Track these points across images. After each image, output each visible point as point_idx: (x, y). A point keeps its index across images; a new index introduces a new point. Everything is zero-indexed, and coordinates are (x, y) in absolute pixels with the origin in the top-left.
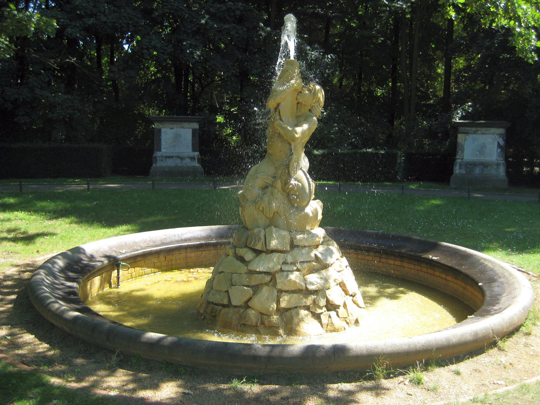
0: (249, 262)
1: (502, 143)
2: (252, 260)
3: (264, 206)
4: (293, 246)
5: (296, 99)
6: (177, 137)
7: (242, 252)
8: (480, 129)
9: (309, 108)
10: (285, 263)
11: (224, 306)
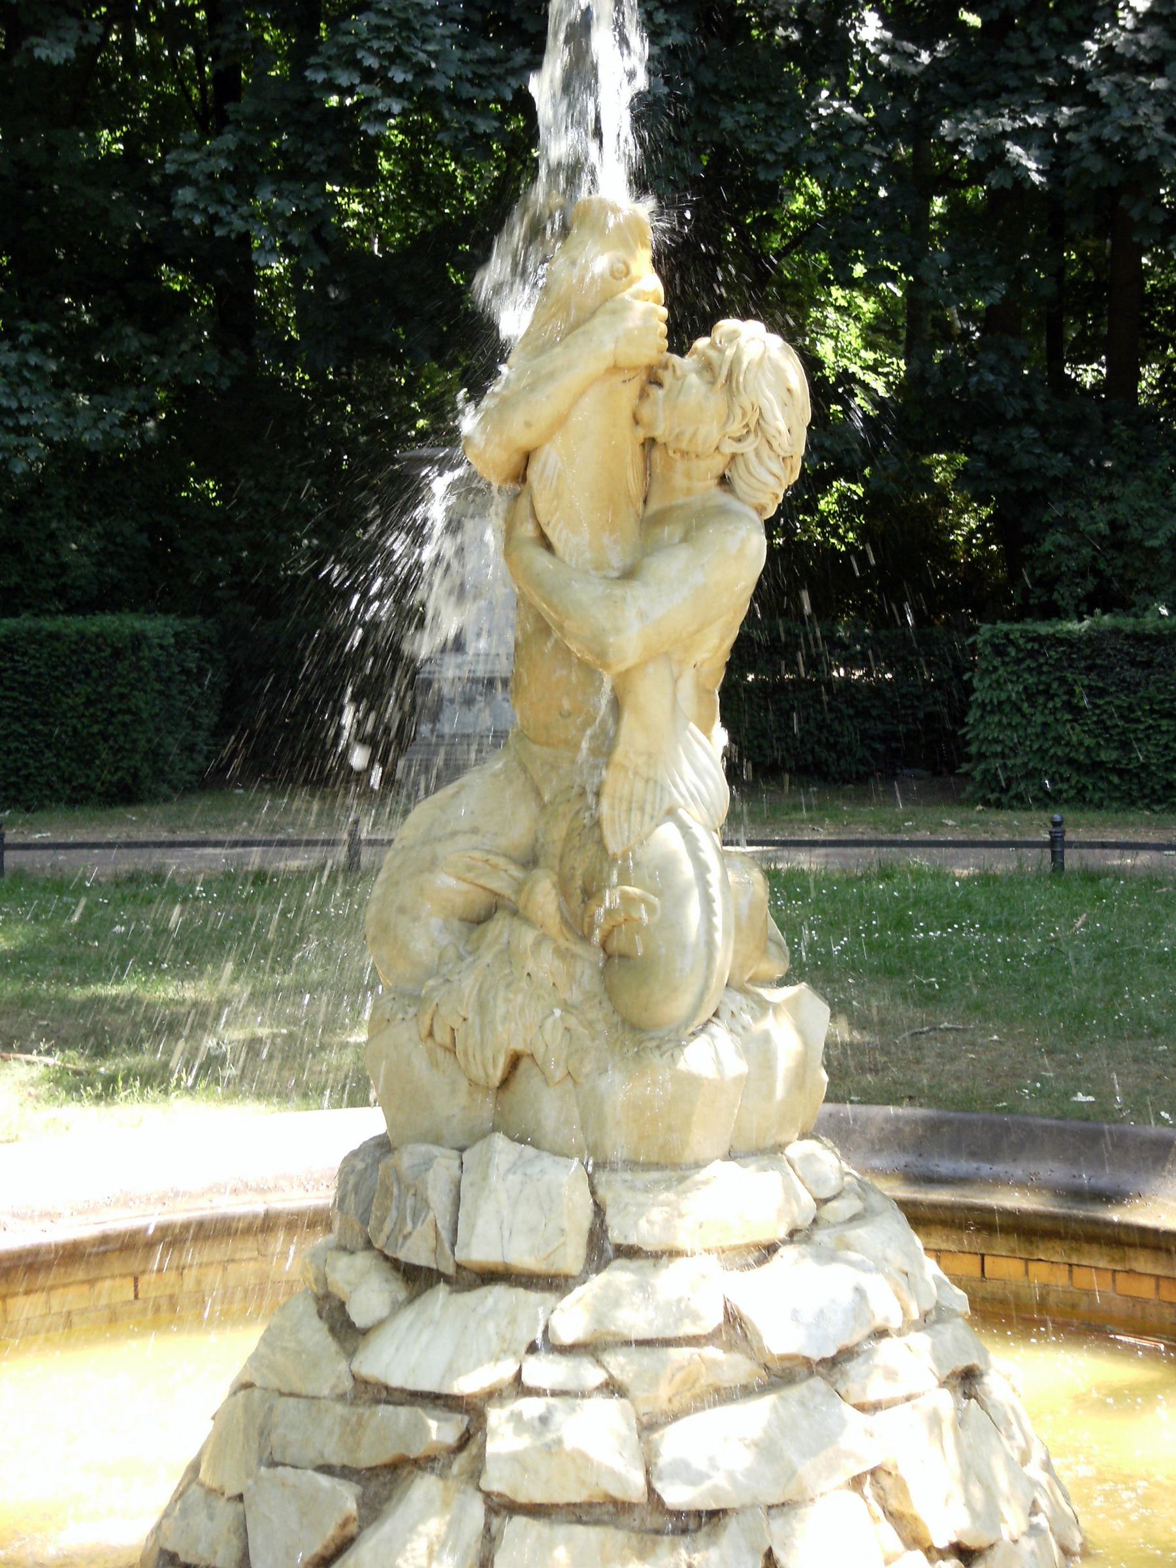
0: (365, 1332)
3: (457, 1023)
4: (602, 1249)
5: (636, 421)
9: (717, 464)
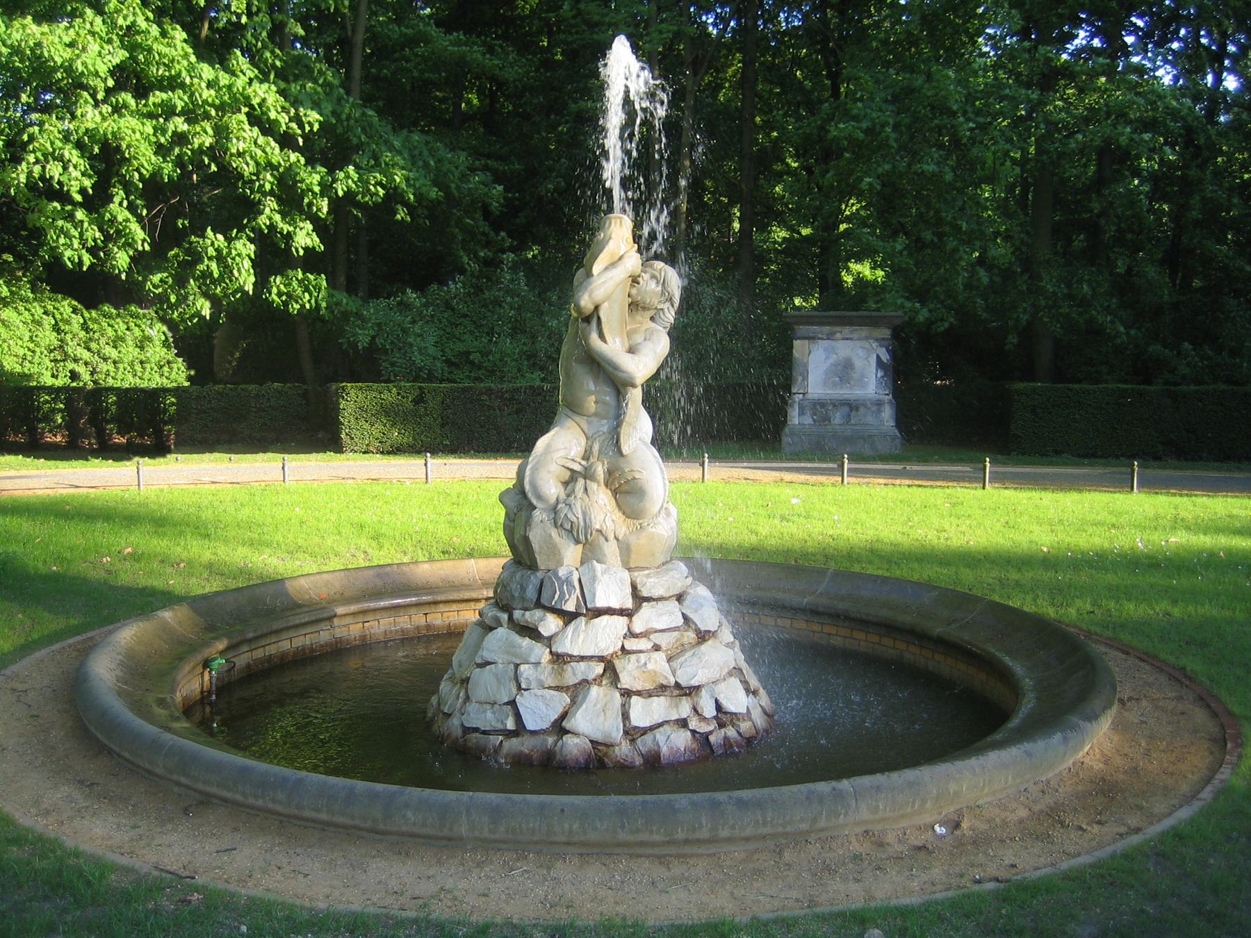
1: (885, 357)
2: (556, 634)
6: (844, 372)
7: (532, 616)
8: (838, 329)
10: (631, 634)
11: (509, 734)
